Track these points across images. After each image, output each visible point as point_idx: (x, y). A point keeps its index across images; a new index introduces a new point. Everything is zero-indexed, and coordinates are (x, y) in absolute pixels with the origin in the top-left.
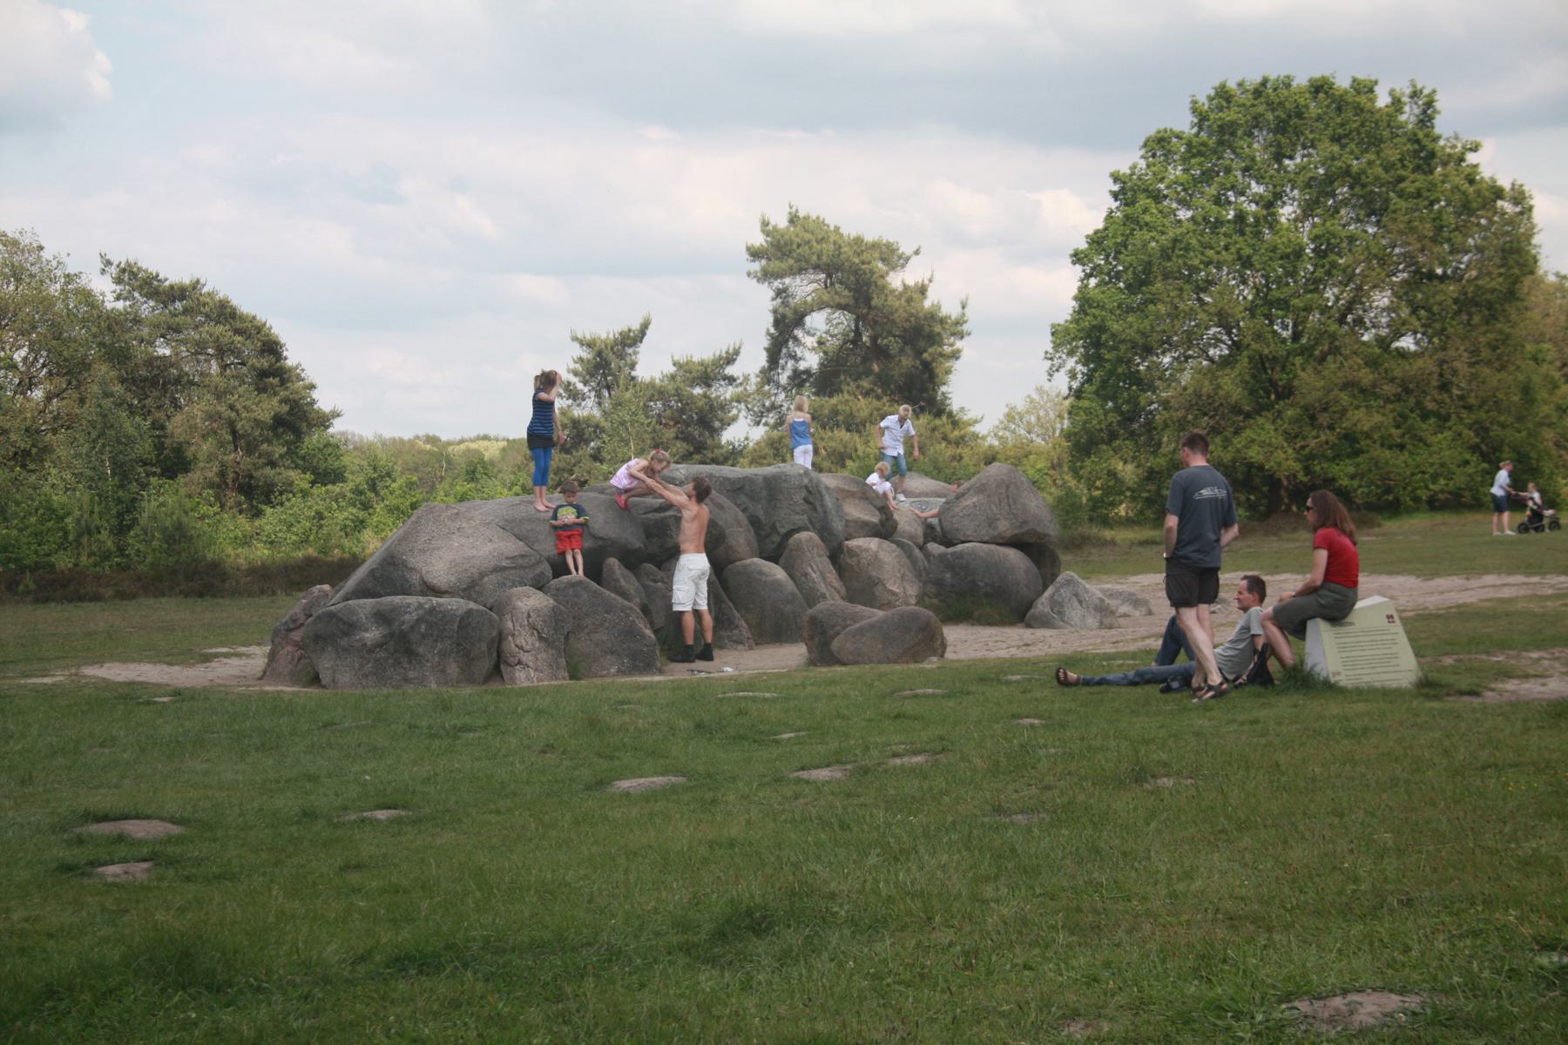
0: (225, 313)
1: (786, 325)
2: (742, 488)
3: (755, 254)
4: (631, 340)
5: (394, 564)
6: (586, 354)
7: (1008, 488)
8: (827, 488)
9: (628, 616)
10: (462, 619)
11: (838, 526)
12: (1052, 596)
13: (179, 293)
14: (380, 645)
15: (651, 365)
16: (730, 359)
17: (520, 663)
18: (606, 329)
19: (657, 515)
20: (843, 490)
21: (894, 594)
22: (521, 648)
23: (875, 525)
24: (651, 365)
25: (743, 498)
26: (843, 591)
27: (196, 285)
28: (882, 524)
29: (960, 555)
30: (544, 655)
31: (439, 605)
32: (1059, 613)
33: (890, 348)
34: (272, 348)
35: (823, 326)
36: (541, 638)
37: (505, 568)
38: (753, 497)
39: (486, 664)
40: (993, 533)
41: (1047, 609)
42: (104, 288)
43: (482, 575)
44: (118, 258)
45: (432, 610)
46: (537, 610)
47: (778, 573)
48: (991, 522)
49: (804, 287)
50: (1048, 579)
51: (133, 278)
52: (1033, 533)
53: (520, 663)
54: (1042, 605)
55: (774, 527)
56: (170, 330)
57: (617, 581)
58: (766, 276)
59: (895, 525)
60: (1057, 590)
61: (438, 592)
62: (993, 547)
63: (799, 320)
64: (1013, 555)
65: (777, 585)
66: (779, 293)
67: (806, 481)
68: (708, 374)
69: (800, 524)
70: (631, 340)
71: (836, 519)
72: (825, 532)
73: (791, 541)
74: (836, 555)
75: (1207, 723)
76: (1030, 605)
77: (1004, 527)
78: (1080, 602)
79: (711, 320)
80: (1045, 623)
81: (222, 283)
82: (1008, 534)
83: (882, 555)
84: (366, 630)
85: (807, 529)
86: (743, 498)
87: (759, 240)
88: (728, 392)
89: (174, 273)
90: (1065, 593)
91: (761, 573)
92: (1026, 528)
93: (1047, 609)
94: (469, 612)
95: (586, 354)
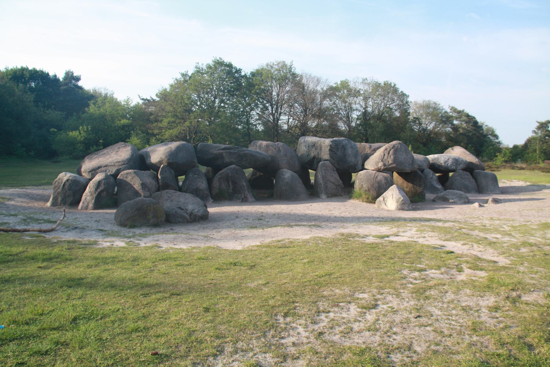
0: (468, 116)
13: (459, 112)
18: (543, 120)
27: (463, 111)
42: (449, 111)
44: (451, 106)
51: (454, 110)
89: (460, 108)
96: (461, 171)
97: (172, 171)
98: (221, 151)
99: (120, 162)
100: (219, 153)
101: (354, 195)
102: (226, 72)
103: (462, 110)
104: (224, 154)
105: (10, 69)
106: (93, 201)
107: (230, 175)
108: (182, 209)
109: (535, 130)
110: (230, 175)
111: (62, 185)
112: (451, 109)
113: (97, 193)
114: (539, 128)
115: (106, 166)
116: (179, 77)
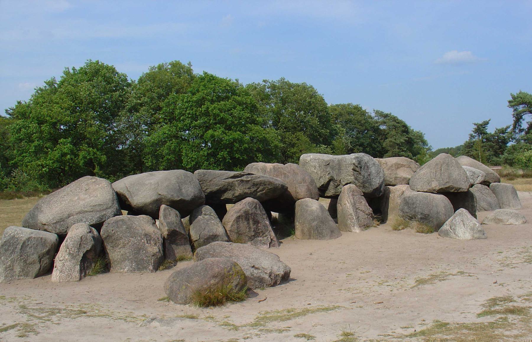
0: (395, 119)
3: (510, 102)
4: (486, 123)
10: (24, 243)
13: (386, 116)
15: (491, 130)
24: (491, 130)
25: (329, 169)
27: (390, 114)
30: (68, 263)
34: (405, 126)
40: (429, 188)
42: (373, 115)
49: (521, 108)
51: (380, 114)
56: (384, 123)
58: (512, 106)
63: (521, 117)
64: (441, 197)
66: (515, 110)
68: (503, 131)
70: (486, 123)
75: (123, 251)
77: (435, 185)
78: (464, 225)
82: (437, 188)
87: (511, 99)
89: (386, 112)
91: (307, 206)
93: (448, 228)
95: (476, 127)
96: (480, 185)
97: (177, 212)
98: (231, 180)
99: (100, 205)
100: (229, 183)
101: (298, 232)
102: (99, 75)
103: (389, 113)
104: (236, 183)
105: (78, 68)
106: (78, 268)
107: (250, 212)
108: (257, 268)
109: (472, 133)
110: (250, 212)
111: (19, 247)
112: (376, 113)
113: (82, 255)
115: (80, 213)
116: (43, 85)
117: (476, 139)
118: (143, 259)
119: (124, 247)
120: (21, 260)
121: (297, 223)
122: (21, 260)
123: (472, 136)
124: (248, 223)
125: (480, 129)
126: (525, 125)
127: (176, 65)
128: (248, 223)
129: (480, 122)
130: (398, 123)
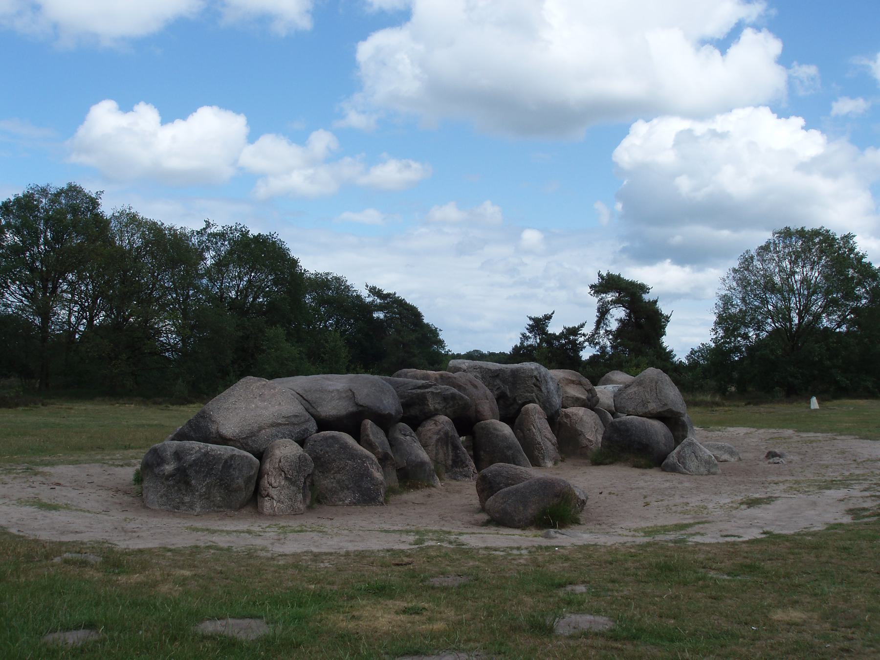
1: (603, 312)
2: (498, 376)
4: (548, 318)
5: (203, 417)
6: (531, 323)
7: (657, 383)
8: (552, 378)
9: (364, 462)
10: (226, 462)
11: (557, 401)
12: (679, 453)
13: (388, 295)
14: (171, 475)
15: (555, 328)
16: (582, 326)
17: (268, 495)
19: (419, 391)
20: (567, 379)
21: (590, 441)
22: (271, 485)
23: (584, 400)
25: (498, 382)
26: (554, 440)
28: (589, 399)
29: (624, 423)
30: (286, 491)
31: (212, 450)
32: (683, 463)
33: (643, 321)
35: (618, 313)
36: (286, 478)
37: (280, 424)
38: (504, 381)
39: (244, 495)
41: (676, 460)
42: (364, 293)
43: (260, 429)
44: (370, 284)
45: (206, 454)
46: (285, 457)
47: (506, 429)
48: (644, 403)
49: (610, 297)
50: (678, 440)
51: (374, 291)
52: (670, 411)
53: (268, 495)
54: (673, 457)
55: (515, 400)
56: (380, 308)
57: (368, 436)
59: (598, 401)
60: (683, 449)
61: (223, 440)
62: (644, 419)
63: (608, 311)
65: (505, 438)
67: (535, 373)
68: (574, 331)
69: (530, 399)
70: (548, 318)
71: (556, 397)
72: (546, 404)
73: (523, 409)
74: (553, 419)
76: (665, 456)
77: (653, 407)
78: (696, 457)
79: (574, 309)
80: (673, 469)
81: (401, 294)
83: (585, 418)
84: (168, 464)
85: (534, 402)
86: (498, 382)
88: (582, 339)
90: (688, 451)
91: (495, 429)
92: (666, 408)
93: (676, 460)
94: (232, 457)
95: (531, 323)
99: (296, 416)
103: (392, 292)
112: (370, 291)
114: (532, 329)
117: (531, 342)
118: (369, 488)
119: (338, 472)
120: (221, 485)
121: (482, 453)
122: (221, 485)
123: (525, 337)
124: (447, 449)
125: (539, 325)
126: (614, 326)
127: (73, 191)
128: (447, 449)
129: (540, 315)
130: (407, 309)
